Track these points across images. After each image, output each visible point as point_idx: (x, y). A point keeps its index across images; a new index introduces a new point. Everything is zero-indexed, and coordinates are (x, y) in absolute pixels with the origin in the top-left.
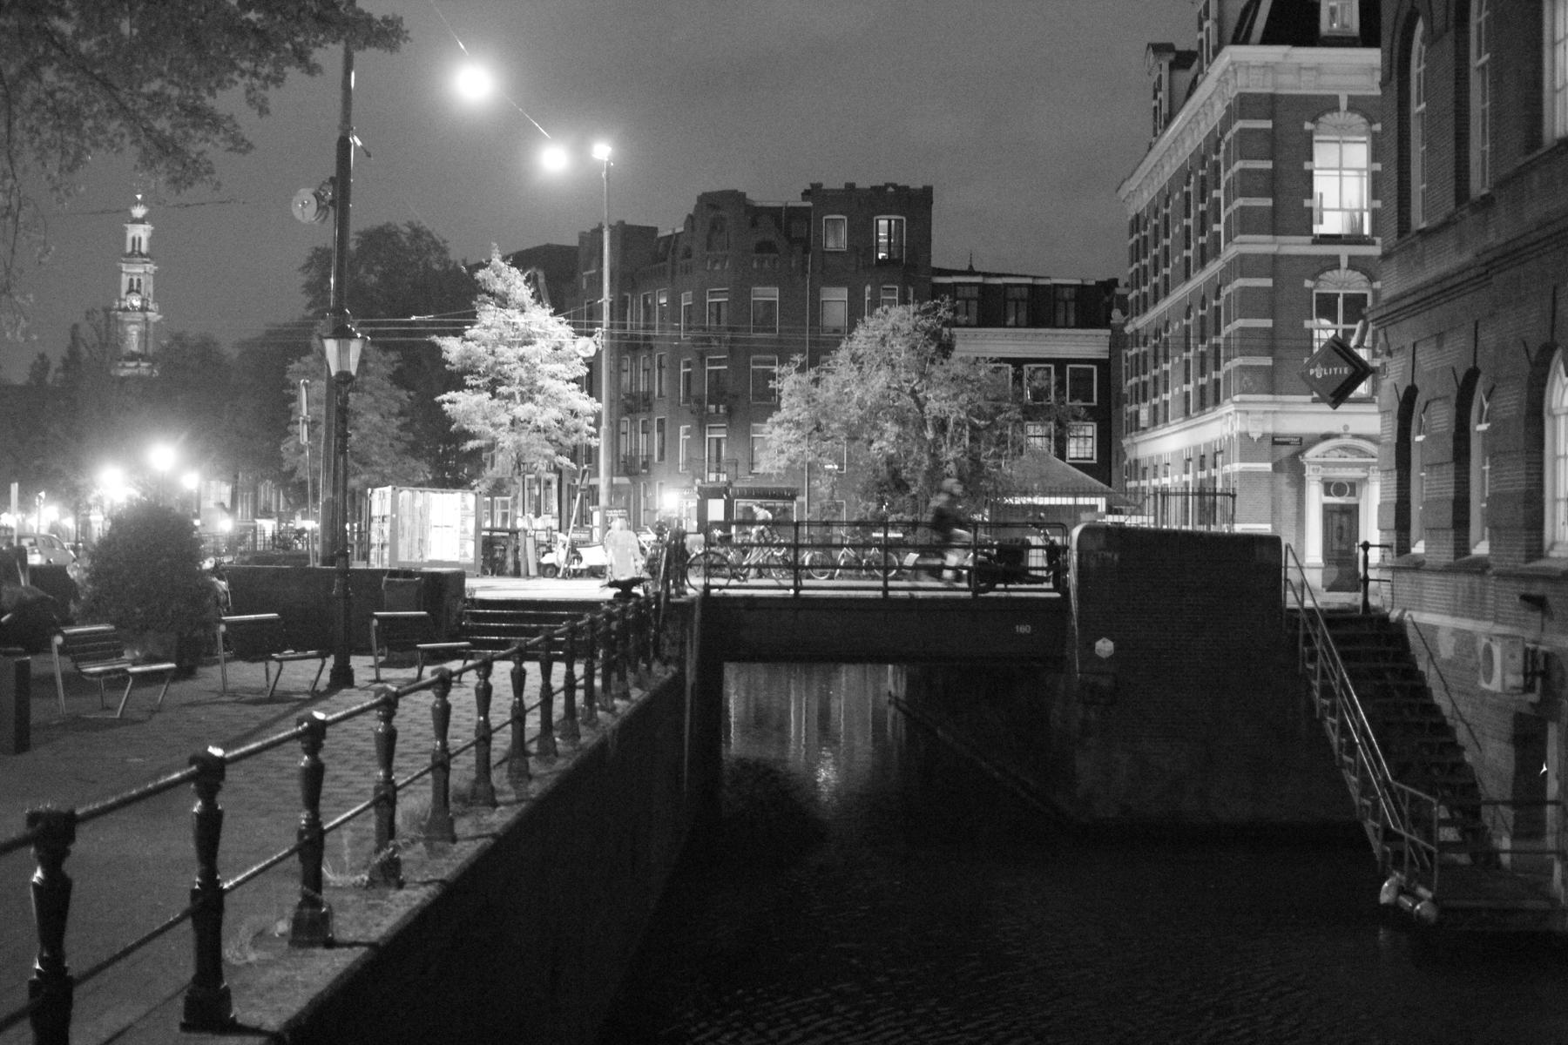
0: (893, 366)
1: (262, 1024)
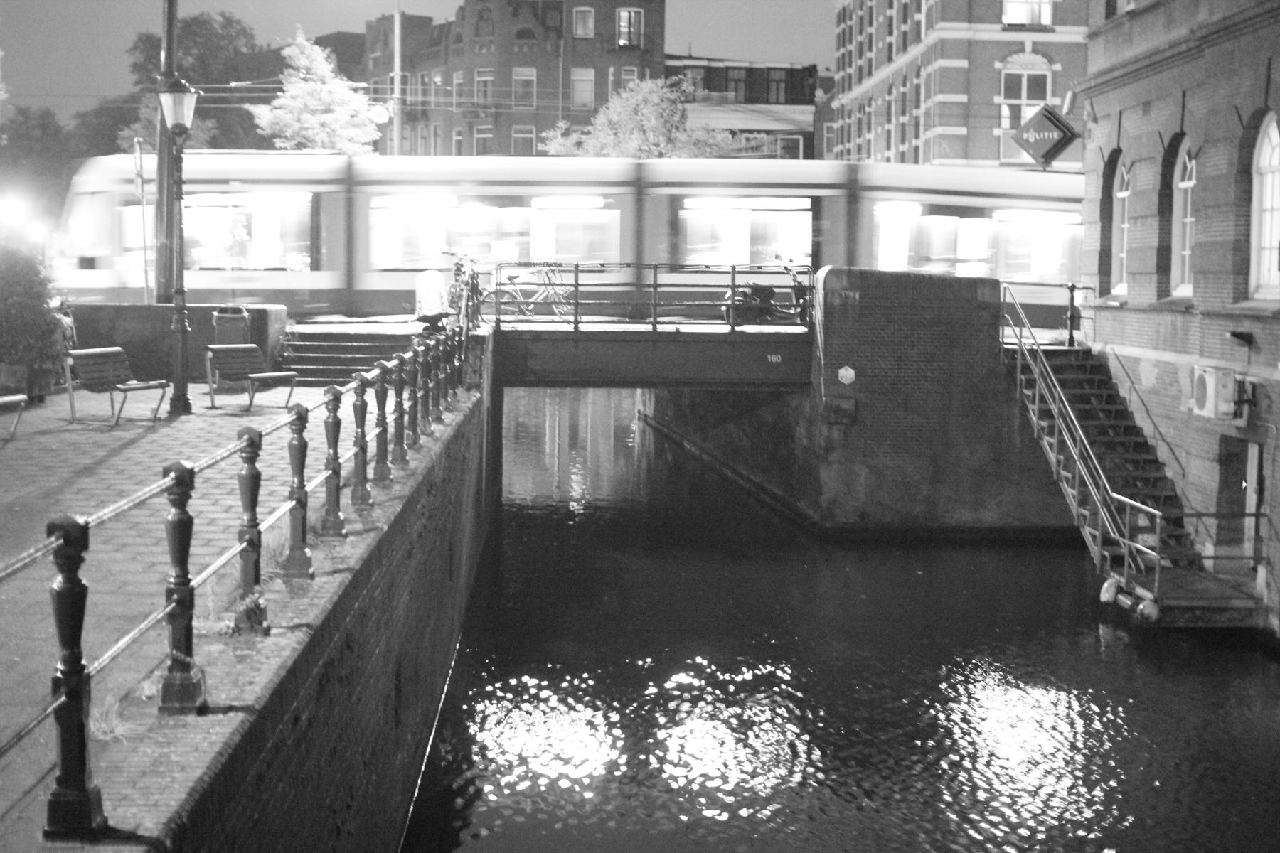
0: (644, 132)
1: (138, 826)
